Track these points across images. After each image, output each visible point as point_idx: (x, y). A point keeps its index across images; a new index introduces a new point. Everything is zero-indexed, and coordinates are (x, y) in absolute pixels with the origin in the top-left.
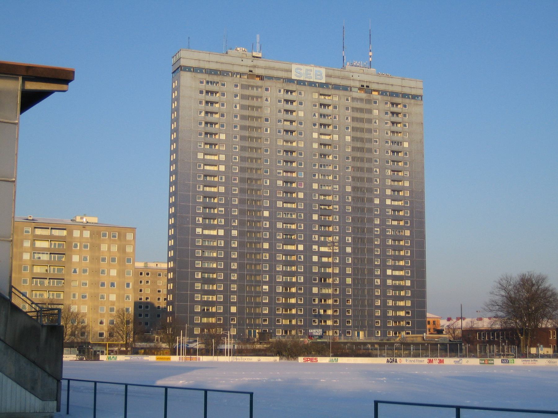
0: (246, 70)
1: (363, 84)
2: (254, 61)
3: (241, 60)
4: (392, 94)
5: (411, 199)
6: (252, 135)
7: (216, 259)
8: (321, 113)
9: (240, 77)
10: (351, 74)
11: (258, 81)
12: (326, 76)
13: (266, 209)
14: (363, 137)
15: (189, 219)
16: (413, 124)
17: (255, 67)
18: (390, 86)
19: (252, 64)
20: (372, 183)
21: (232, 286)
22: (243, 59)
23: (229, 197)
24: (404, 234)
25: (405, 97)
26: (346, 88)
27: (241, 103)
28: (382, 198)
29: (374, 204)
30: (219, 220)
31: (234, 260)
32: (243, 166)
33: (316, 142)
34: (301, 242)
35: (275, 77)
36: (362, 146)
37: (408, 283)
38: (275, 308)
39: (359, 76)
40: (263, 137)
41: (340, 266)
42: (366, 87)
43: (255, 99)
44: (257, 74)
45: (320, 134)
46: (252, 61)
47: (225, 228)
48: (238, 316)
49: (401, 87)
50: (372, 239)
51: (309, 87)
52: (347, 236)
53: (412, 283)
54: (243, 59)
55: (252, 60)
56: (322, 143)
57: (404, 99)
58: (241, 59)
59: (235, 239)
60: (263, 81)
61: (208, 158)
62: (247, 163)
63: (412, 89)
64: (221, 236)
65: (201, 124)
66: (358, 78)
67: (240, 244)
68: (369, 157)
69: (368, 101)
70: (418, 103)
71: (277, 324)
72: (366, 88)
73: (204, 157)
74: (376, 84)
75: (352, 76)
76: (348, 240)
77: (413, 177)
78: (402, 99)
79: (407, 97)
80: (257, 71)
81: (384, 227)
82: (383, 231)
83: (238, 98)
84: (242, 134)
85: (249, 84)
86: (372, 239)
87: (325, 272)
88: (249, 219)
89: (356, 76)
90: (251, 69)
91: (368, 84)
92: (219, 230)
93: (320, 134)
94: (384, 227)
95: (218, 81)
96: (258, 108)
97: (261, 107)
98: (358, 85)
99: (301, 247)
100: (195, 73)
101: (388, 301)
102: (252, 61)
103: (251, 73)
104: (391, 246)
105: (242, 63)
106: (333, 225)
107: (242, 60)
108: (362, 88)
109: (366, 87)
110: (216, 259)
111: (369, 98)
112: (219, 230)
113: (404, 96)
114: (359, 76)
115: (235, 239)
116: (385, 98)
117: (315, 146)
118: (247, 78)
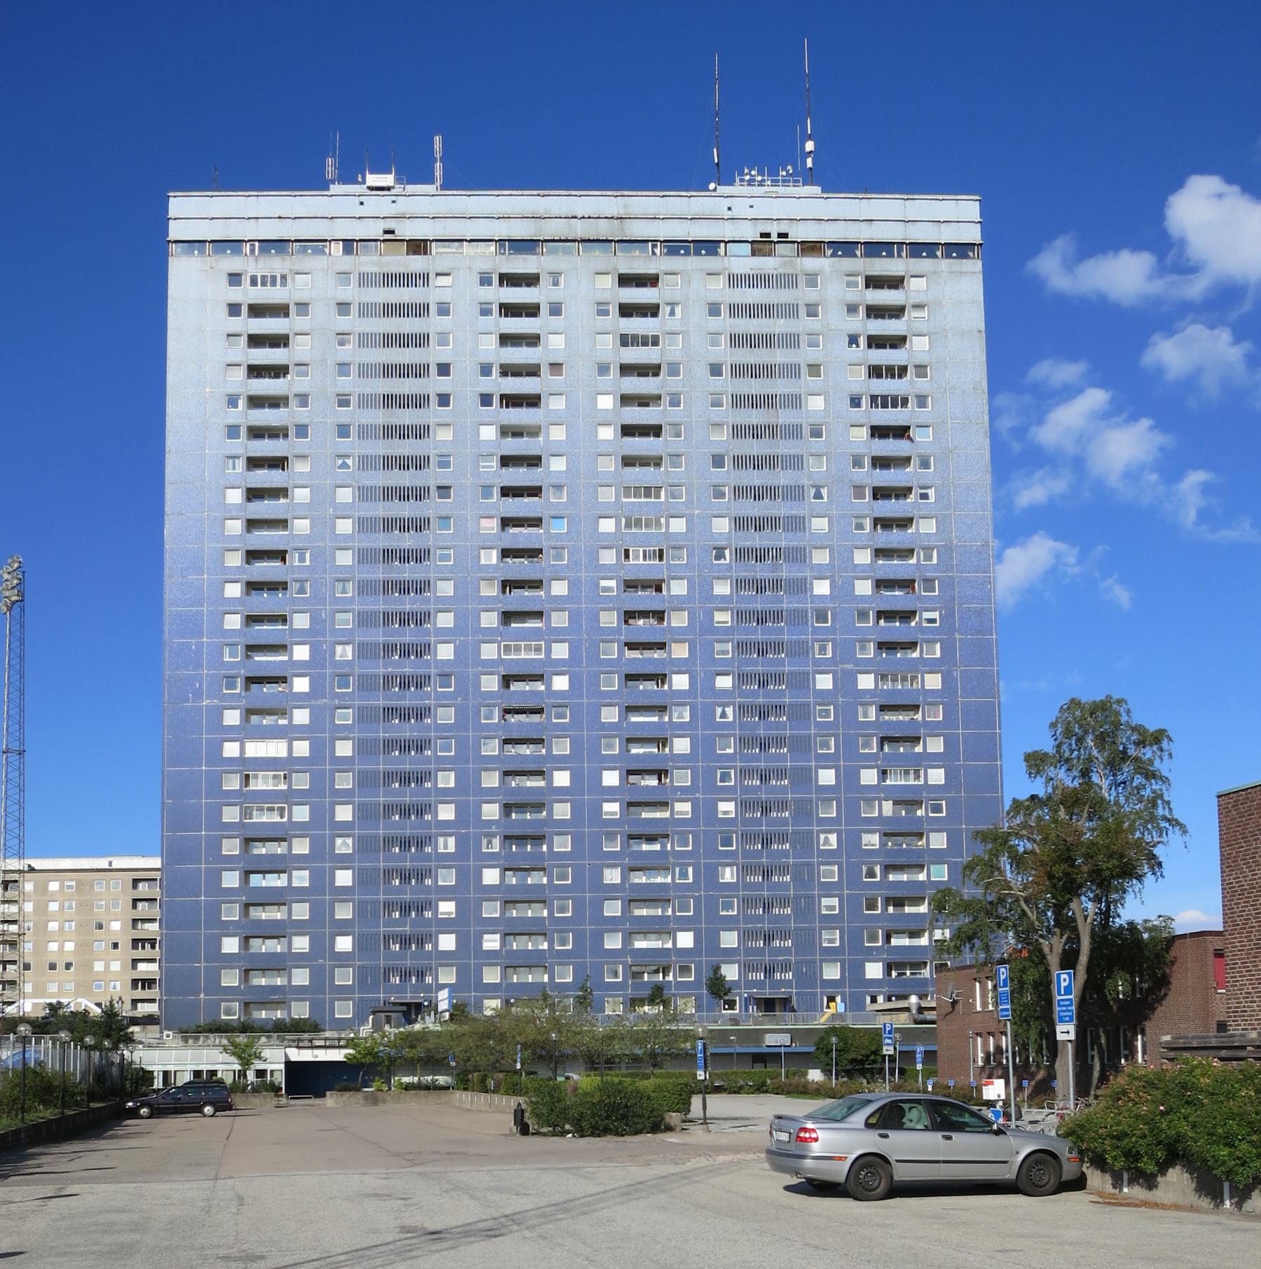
5: (945, 572)
15: (201, 684)
41: (697, 795)
60: (431, 257)
63: (943, 225)
85: (386, 270)
88: (390, 670)
91: (783, 228)
102: (394, 202)
107: (362, 203)
111: (790, 271)
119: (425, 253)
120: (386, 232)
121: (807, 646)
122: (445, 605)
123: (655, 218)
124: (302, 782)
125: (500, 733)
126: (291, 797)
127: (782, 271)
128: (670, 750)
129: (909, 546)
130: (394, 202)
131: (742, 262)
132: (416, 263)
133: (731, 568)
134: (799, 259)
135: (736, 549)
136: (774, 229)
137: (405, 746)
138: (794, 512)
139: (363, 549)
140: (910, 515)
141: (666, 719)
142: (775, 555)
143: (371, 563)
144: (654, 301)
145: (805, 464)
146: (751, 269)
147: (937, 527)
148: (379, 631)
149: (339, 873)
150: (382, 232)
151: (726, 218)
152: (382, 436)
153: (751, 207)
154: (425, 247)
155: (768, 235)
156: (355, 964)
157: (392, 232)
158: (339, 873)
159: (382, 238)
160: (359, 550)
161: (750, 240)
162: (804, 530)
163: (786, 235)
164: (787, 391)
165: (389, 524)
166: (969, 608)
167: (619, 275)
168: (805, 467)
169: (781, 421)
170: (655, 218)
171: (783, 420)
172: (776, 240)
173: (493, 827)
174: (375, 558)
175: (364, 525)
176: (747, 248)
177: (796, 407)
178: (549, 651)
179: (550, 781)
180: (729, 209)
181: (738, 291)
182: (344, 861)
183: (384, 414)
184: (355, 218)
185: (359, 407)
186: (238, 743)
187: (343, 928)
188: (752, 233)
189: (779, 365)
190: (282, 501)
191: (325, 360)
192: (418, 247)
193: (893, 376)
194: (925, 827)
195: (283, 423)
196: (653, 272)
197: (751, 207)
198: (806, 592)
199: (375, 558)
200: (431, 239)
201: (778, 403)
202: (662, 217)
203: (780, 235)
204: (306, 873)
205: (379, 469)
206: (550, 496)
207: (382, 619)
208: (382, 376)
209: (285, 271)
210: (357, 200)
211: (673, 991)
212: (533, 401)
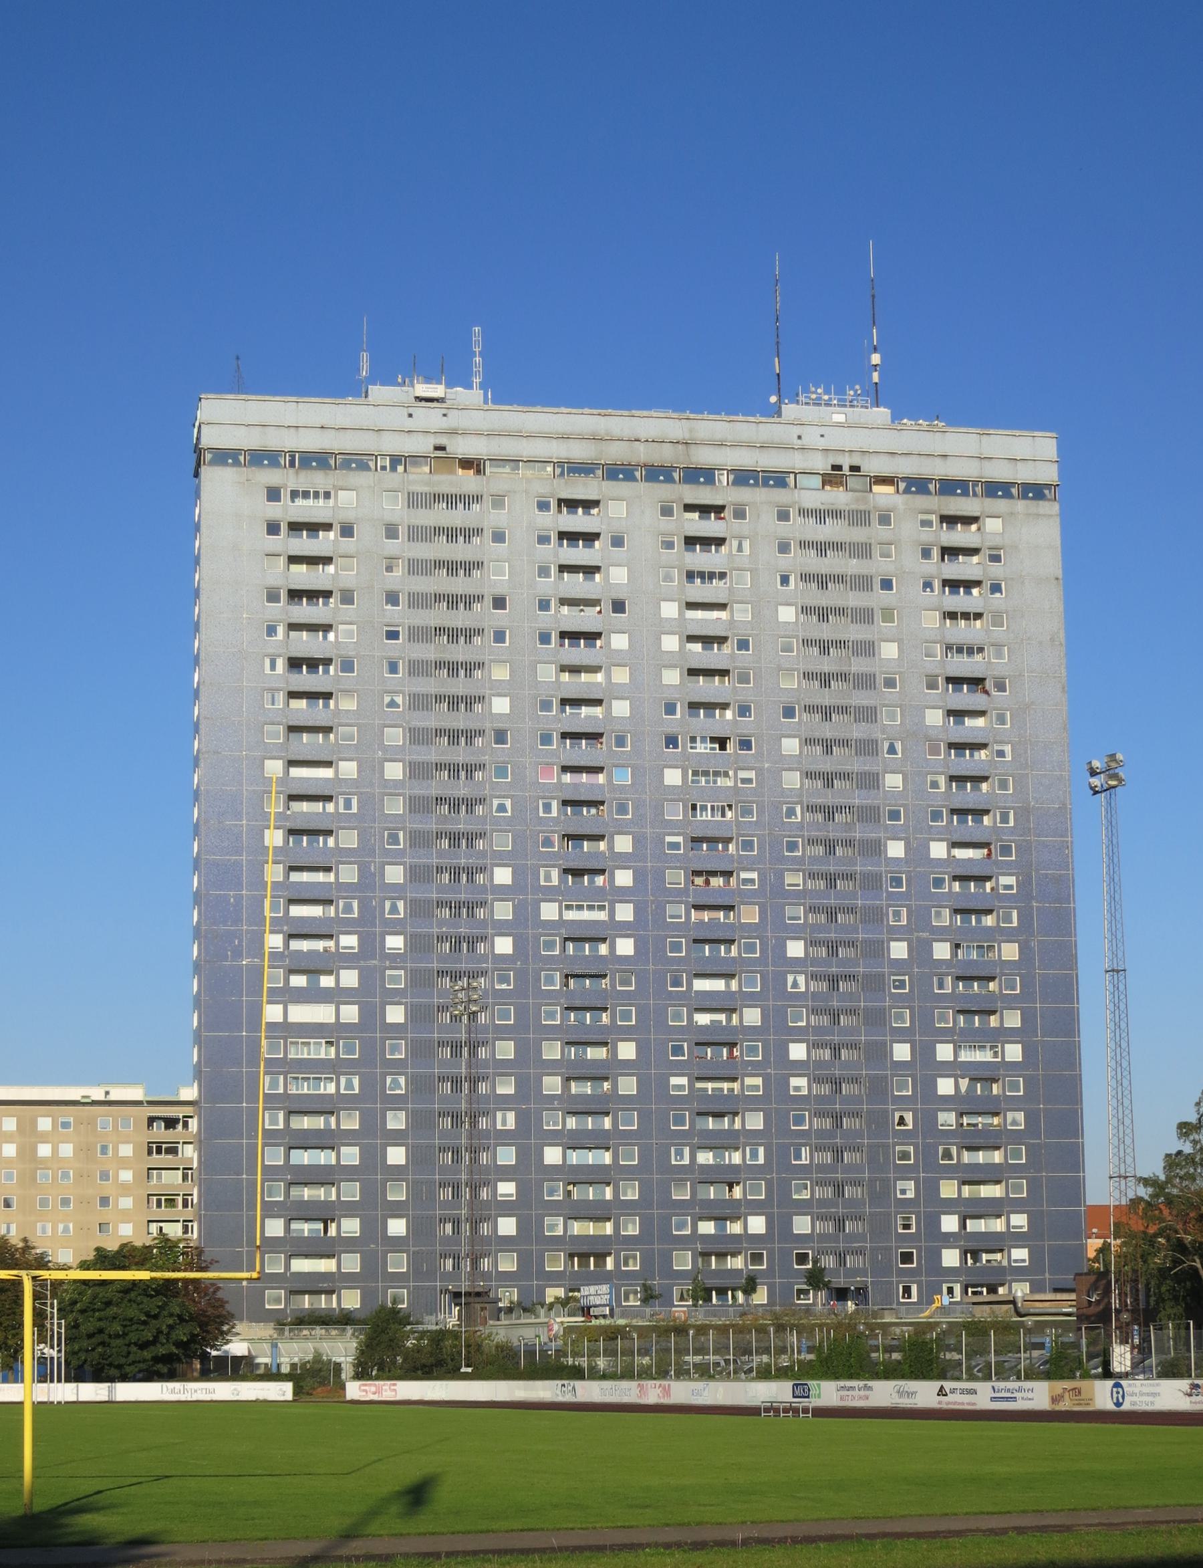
0: (423, 446)
2: (449, 415)
3: (406, 414)
4: (950, 487)
7: (333, 1068)
8: (691, 568)
9: (405, 470)
10: (796, 430)
11: (466, 481)
13: (503, 928)
15: (241, 941)
16: (1023, 583)
17: (453, 432)
18: (938, 461)
19: (444, 424)
20: (876, 791)
21: (391, 1151)
22: (411, 410)
23: (375, 862)
24: (1000, 956)
25: (994, 495)
26: (778, 479)
28: (916, 838)
29: (887, 859)
30: (343, 1080)
31: (396, 1067)
33: (675, 666)
34: (627, 1034)
35: (525, 460)
36: (832, 602)
37: (1020, 1221)
38: (537, 938)
39: (822, 436)
40: (486, 662)
41: (769, 1071)
42: (851, 471)
43: (462, 673)
44: (460, 457)
45: (694, 940)
46: (445, 415)
47: (362, 963)
48: (412, 1249)
49: (976, 462)
50: (882, 1011)
51: (647, 484)
52: (792, 972)
53: (1030, 1118)
54: (411, 410)
55: (445, 411)
56: (699, 833)
57: (988, 501)
58: (405, 412)
59: (396, 999)
60: (485, 478)
61: (305, 880)
62: (433, 644)
63: (1019, 463)
64: (351, 1277)
65: (271, 631)
66: (822, 444)
67: (415, 1190)
68: (865, 703)
69: (860, 518)
70: (1041, 511)
71: (543, 953)
72: (848, 473)
73: (287, 1157)
74: (886, 458)
75: (799, 437)
76: (795, 985)
77: (1027, 763)
78: (982, 503)
79: (1000, 493)
80: (463, 447)
81: (925, 935)
83: (399, 572)
84: (415, 656)
86: (882, 1011)
87: (720, 1198)
88: (444, 929)
89: (811, 437)
90: (442, 441)
91: (856, 461)
93: (694, 940)
94: (925, 935)
95: (329, 488)
96: (469, 567)
97: (479, 565)
98: (822, 464)
99: (627, 1051)
100: (250, 470)
103: (440, 454)
104: (953, 996)
105: (409, 424)
106: (742, 972)
107: (410, 415)
108: (833, 477)
109: (851, 471)
110: (333, 1068)
111: (862, 507)
113: (996, 489)
114: (822, 436)
115: (396, 999)
116: (921, 501)
117: (672, 677)
118: (428, 472)
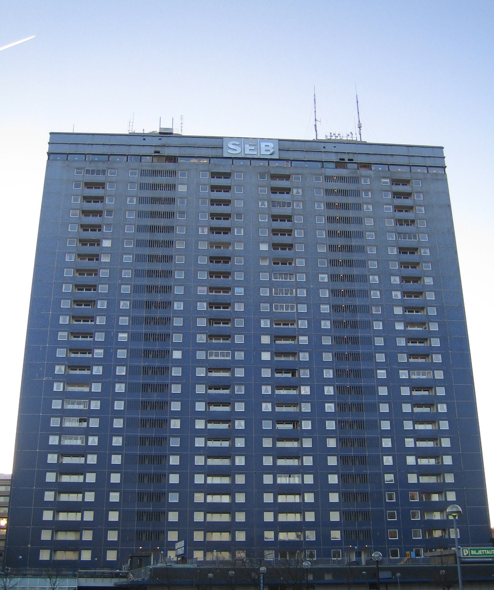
1: (343, 157)
5: (441, 319)
6: (156, 238)
12: (279, 150)
14: (352, 288)
15: (43, 369)
19: (159, 143)
27: (139, 195)
32: (138, 283)
41: (316, 435)
50: (376, 421)
60: (177, 164)
63: (427, 159)
66: (334, 150)
82: (394, 390)
85: (154, 169)
86: (376, 421)
88: (147, 364)
91: (351, 157)
92: (305, 476)
101: (279, 540)
102: (160, 139)
107: (144, 139)
111: (355, 176)
112: (305, 476)
119: (175, 162)
120: (155, 152)
121: (372, 356)
122: (180, 283)
123: (288, 150)
124: (94, 423)
125: (206, 399)
126: (88, 432)
127: (351, 175)
128: (298, 359)
129: (422, 306)
130: (160, 139)
131: (332, 171)
132: (170, 166)
133: (331, 315)
134: (359, 170)
135: (333, 305)
136: (346, 157)
137: (153, 406)
138: (362, 288)
139: (140, 226)
140: (422, 291)
141: (297, 359)
142: (353, 308)
143: (139, 308)
144: (288, 187)
145: (367, 265)
146: (336, 174)
147: (428, 239)
148: (143, 310)
149: (113, 475)
150: (153, 152)
151: (323, 151)
152: (148, 245)
153: (335, 147)
154: (175, 159)
155: (344, 160)
156: (132, 284)
157: (159, 152)
158: (113, 475)
159: (153, 155)
160: (134, 285)
161: (335, 161)
162: (368, 297)
163: (352, 160)
164: (355, 230)
165: (150, 273)
166: (454, 337)
167: (271, 174)
168: (367, 266)
169: (353, 244)
170: (288, 150)
171: (355, 243)
172: (347, 161)
173: (201, 451)
174: (142, 306)
175: (138, 273)
176: (333, 165)
177: (361, 238)
178: (233, 356)
179: (233, 373)
180: (324, 147)
181: (332, 211)
182: (120, 379)
183: (150, 234)
184: (141, 145)
185: (138, 232)
186: (55, 473)
187: (116, 450)
188: (334, 158)
189: (352, 218)
190: (89, 339)
191: (122, 209)
192: (172, 159)
193: (408, 225)
194: (435, 401)
195: (98, 238)
196: (288, 173)
197: (335, 147)
198: (370, 328)
199: (142, 306)
200: (178, 155)
201: (352, 235)
202: (291, 150)
203: (349, 160)
204: (95, 457)
205: (146, 261)
206: (234, 219)
207: (144, 337)
208: (150, 217)
209: (105, 168)
210: (142, 138)
211: (304, 547)
212: (227, 231)
